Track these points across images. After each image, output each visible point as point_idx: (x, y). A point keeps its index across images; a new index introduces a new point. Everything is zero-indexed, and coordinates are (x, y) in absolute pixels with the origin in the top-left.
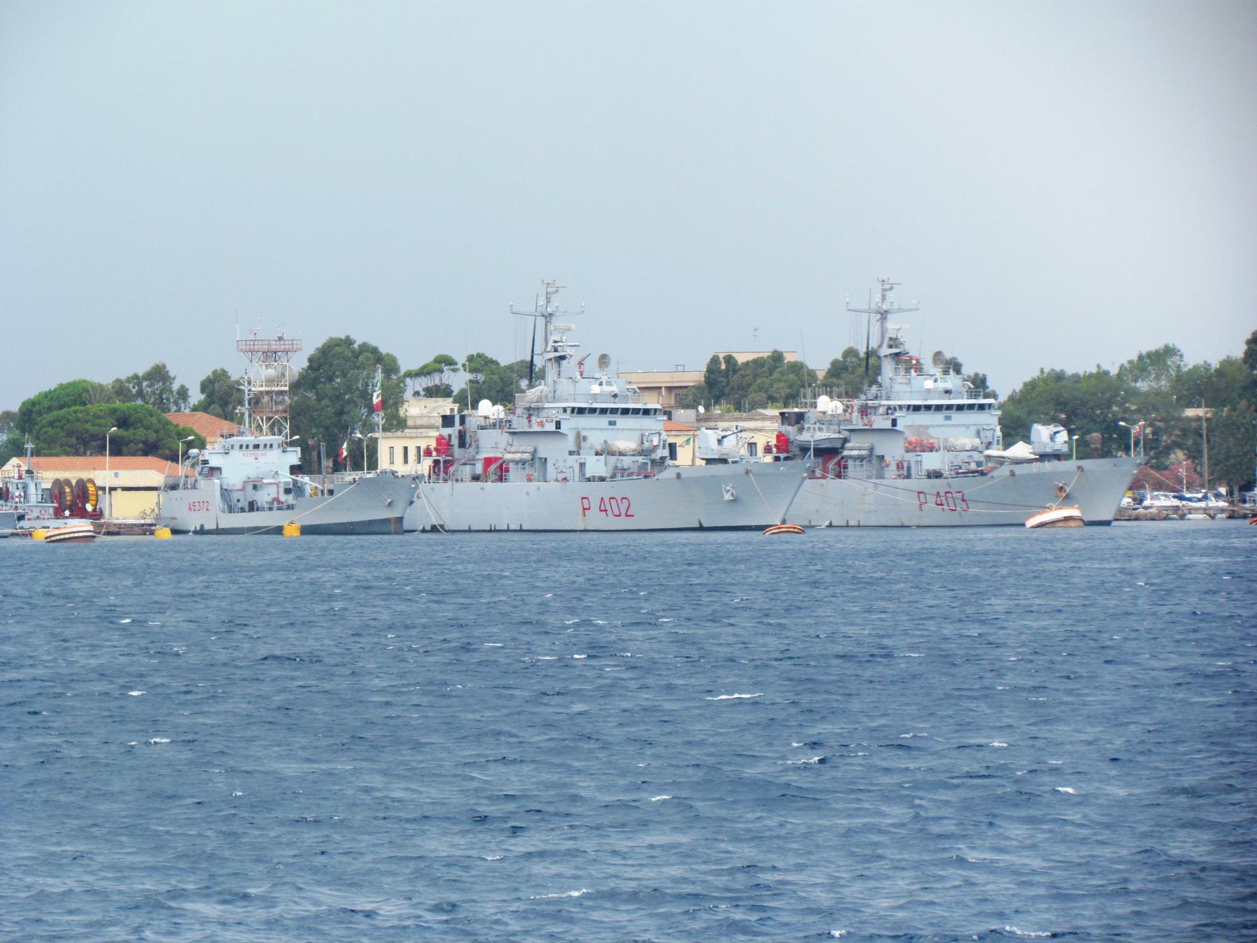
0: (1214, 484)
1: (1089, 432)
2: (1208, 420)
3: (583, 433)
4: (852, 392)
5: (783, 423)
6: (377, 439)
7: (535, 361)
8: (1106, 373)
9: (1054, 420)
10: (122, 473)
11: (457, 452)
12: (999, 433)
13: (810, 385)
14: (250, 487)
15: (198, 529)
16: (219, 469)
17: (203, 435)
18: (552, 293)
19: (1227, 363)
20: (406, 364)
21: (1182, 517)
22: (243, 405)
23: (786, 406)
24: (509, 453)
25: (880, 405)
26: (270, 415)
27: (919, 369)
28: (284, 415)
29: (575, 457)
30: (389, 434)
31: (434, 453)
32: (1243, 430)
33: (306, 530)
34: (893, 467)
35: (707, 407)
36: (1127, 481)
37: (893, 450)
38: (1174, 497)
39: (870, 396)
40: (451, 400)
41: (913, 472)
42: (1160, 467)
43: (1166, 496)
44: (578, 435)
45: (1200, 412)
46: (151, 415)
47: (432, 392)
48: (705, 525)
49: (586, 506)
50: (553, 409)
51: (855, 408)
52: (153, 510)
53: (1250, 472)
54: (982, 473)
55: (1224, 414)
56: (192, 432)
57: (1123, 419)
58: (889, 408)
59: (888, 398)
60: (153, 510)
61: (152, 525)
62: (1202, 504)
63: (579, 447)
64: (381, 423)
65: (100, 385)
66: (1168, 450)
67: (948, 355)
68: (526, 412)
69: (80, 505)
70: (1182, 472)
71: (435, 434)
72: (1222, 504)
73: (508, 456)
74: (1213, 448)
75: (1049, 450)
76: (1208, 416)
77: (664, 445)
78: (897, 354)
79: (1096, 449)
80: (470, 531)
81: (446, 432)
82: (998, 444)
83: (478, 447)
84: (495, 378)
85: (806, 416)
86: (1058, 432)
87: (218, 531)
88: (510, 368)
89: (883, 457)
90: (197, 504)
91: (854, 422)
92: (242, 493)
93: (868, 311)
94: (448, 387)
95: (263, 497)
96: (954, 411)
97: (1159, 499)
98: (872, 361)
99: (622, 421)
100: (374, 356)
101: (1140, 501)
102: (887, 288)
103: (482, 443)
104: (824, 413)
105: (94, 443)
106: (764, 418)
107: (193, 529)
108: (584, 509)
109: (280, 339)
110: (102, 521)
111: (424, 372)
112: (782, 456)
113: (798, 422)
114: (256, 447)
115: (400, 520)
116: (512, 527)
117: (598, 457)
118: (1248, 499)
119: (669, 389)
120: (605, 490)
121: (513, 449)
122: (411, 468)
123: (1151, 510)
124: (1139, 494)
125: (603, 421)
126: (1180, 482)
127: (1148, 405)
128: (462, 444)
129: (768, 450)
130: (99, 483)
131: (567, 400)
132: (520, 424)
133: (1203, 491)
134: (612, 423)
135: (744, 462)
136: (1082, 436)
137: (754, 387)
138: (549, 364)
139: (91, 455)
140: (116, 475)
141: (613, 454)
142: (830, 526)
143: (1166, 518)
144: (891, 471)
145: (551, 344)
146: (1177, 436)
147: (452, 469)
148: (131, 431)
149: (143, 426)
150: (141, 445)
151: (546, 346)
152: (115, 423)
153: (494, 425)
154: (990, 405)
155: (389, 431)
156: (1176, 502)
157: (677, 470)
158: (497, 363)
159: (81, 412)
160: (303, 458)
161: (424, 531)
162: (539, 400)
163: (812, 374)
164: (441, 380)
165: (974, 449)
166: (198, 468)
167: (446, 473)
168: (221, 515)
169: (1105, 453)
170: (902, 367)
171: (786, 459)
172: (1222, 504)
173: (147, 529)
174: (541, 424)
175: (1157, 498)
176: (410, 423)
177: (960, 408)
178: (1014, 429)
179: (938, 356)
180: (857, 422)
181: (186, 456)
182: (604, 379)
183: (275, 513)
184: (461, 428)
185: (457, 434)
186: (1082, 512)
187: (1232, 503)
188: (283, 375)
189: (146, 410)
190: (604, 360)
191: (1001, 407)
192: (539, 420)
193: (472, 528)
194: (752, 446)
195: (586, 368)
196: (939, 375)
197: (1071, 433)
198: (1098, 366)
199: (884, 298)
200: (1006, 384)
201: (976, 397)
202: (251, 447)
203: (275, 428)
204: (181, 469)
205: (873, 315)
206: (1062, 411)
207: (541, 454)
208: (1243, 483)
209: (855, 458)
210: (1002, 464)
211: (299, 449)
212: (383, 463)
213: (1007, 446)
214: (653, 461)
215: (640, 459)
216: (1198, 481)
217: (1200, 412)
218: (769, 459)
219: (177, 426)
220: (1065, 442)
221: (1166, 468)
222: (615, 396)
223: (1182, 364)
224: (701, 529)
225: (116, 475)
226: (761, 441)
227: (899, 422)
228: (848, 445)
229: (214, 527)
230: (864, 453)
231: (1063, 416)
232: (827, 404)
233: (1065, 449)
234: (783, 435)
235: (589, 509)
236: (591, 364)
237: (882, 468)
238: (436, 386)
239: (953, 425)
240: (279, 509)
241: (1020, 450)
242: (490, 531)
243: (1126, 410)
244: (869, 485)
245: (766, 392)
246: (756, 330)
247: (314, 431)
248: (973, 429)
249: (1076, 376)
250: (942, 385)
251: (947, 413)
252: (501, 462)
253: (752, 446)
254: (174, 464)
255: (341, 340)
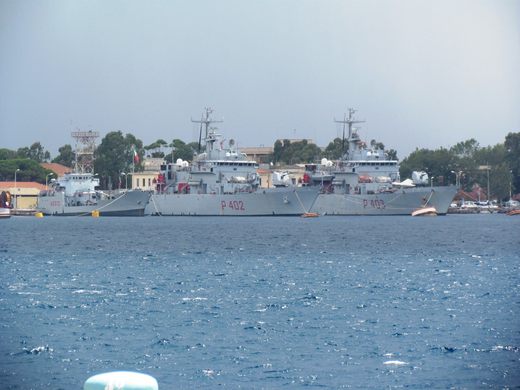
0: (492, 198)
1: (438, 175)
2: (489, 170)
3: (223, 174)
4: (335, 157)
5: (306, 170)
6: (131, 176)
7: (201, 144)
8: (446, 150)
9: (423, 170)
10: (21, 189)
11: (167, 181)
12: (399, 175)
13: (318, 154)
14: (77, 195)
15: (55, 213)
16: (64, 188)
17: (57, 173)
18: (209, 113)
19: (498, 147)
20: (146, 143)
21: (479, 212)
22: (75, 160)
23: (308, 163)
24: (190, 181)
25: (348, 163)
26: (85, 164)
27: (365, 146)
28: (92, 165)
29: (219, 184)
30: (137, 173)
31: (157, 182)
32: (504, 175)
33: (102, 214)
34: (353, 189)
35: (274, 163)
36: (453, 197)
37: (353, 182)
38: (475, 204)
39: (344, 159)
40: (163, 159)
41: (362, 191)
42: (469, 191)
43: (471, 203)
44: (220, 174)
45: (486, 167)
46: (34, 164)
47: (155, 155)
48: (275, 214)
49: (224, 205)
50: (210, 163)
51: (338, 164)
52: (35, 205)
53: (507, 193)
54: (391, 192)
55: (496, 168)
56: (51, 172)
57: (453, 170)
58: (352, 164)
59: (352, 160)
60: (35, 205)
61: (34, 211)
62: (487, 207)
63: (221, 179)
64: (134, 168)
65: (11, 151)
66: (472, 183)
67: (378, 141)
68: (198, 164)
69: (3, 202)
70: (479, 193)
71: (158, 173)
72: (495, 207)
73: (190, 183)
74: (491, 183)
75: (419, 183)
76: (489, 168)
77: (258, 179)
78: (356, 141)
79: (441, 183)
80: (173, 215)
81: (163, 172)
82: (398, 180)
83: (176, 179)
84: (183, 150)
85: (317, 167)
86: (424, 175)
87: (64, 215)
88: (190, 145)
89: (349, 185)
90: (54, 203)
91: (337, 170)
92: (74, 198)
93: (344, 122)
94: (163, 153)
95: (83, 200)
96: (379, 166)
97: (468, 204)
98: (345, 144)
99: (239, 169)
100: (132, 139)
101: (459, 205)
102: (351, 112)
103: (178, 178)
104: (324, 166)
105: (9, 176)
106: (299, 168)
107: (53, 213)
108: (223, 206)
109: (90, 132)
110: (13, 209)
111: (152, 147)
112: (306, 184)
113: (313, 169)
114: (80, 178)
115: (143, 210)
116: (191, 214)
117: (229, 184)
118: (506, 204)
119: (258, 155)
120: (232, 198)
121: (192, 180)
122: (146, 188)
123: (465, 209)
124: (460, 202)
125: (231, 168)
126: (478, 197)
127: (463, 164)
128: (170, 178)
129: (300, 181)
130: (12, 193)
131: (215, 159)
132: (195, 169)
133: (487, 201)
134: (235, 169)
135: (290, 186)
136: (435, 178)
137: (294, 155)
138: (208, 144)
139: (8, 181)
140: (19, 190)
141: (236, 182)
142: (326, 214)
143: (472, 213)
144: (352, 191)
145: (208, 135)
146: (476, 177)
147: (165, 189)
148: (26, 171)
149: (31, 169)
150: (30, 177)
151: (206, 136)
152: (18, 167)
153: (184, 170)
154: (395, 163)
155: (137, 172)
156: (475, 206)
157: (264, 190)
158: (184, 143)
159: (4, 162)
160: (100, 184)
161: (153, 215)
162: (204, 159)
163: (319, 149)
164: (159, 150)
165: (388, 182)
166: (55, 187)
167: (162, 190)
168: (65, 207)
169: (445, 184)
170: (358, 146)
171: (308, 185)
172: (496, 207)
173: (31, 213)
174: (204, 169)
175: (467, 204)
176: (146, 169)
177: (382, 164)
178: (405, 174)
179: (373, 142)
180: (338, 170)
181: (49, 182)
182: (232, 150)
183: (88, 206)
184: (169, 171)
185: (167, 173)
186: (436, 210)
187: (500, 206)
188: (91, 147)
189: (32, 162)
190: (232, 142)
191: (400, 164)
192: (203, 168)
193: (174, 214)
194: (294, 180)
195: (223, 145)
196: (373, 150)
197: (430, 176)
198: (441, 147)
199: (350, 117)
200: (403, 155)
201: (389, 159)
202: (78, 178)
203: (87, 170)
204: (47, 188)
205: (346, 124)
206: (427, 166)
207: (204, 182)
208: (504, 198)
209: (337, 185)
210: (399, 188)
211: (99, 179)
212: (134, 186)
213: (402, 180)
214: (253, 186)
215: (247, 185)
216: (485, 197)
217: (486, 167)
218: (300, 185)
219: (45, 169)
220: (427, 179)
221: (471, 191)
222: (236, 157)
223: (478, 147)
224: (274, 215)
225: (19, 190)
226: (297, 177)
227: (356, 170)
228: (334, 180)
229: (62, 212)
230: (340, 183)
231: (427, 168)
232: (326, 162)
233: (427, 182)
234: (306, 175)
235: (225, 206)
236: (226, 144)
237: (349, 190)
238: (157, 153)
239: (380, 172)
240: (90, 205)
241: (408, 182)
242: (181, 215)
243: (454, 166)
244: (343, 197)
245: (300, 157)
246: (295, 130)
247: (104, 172)
248: (388, 174)
249: (432, 151)
250: (375, 154)
251: (377, 166)
252: (187, 185)
253: (294, 180)
254: (45, 185)
255: (116, 132)
